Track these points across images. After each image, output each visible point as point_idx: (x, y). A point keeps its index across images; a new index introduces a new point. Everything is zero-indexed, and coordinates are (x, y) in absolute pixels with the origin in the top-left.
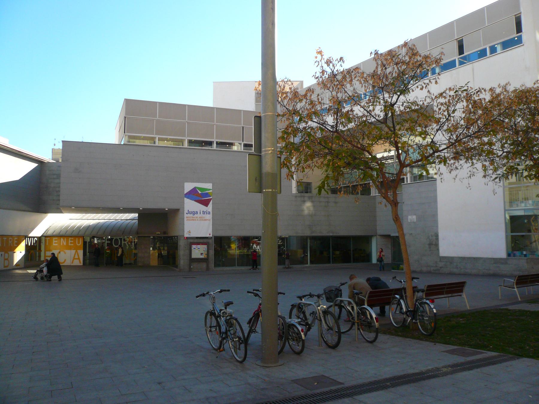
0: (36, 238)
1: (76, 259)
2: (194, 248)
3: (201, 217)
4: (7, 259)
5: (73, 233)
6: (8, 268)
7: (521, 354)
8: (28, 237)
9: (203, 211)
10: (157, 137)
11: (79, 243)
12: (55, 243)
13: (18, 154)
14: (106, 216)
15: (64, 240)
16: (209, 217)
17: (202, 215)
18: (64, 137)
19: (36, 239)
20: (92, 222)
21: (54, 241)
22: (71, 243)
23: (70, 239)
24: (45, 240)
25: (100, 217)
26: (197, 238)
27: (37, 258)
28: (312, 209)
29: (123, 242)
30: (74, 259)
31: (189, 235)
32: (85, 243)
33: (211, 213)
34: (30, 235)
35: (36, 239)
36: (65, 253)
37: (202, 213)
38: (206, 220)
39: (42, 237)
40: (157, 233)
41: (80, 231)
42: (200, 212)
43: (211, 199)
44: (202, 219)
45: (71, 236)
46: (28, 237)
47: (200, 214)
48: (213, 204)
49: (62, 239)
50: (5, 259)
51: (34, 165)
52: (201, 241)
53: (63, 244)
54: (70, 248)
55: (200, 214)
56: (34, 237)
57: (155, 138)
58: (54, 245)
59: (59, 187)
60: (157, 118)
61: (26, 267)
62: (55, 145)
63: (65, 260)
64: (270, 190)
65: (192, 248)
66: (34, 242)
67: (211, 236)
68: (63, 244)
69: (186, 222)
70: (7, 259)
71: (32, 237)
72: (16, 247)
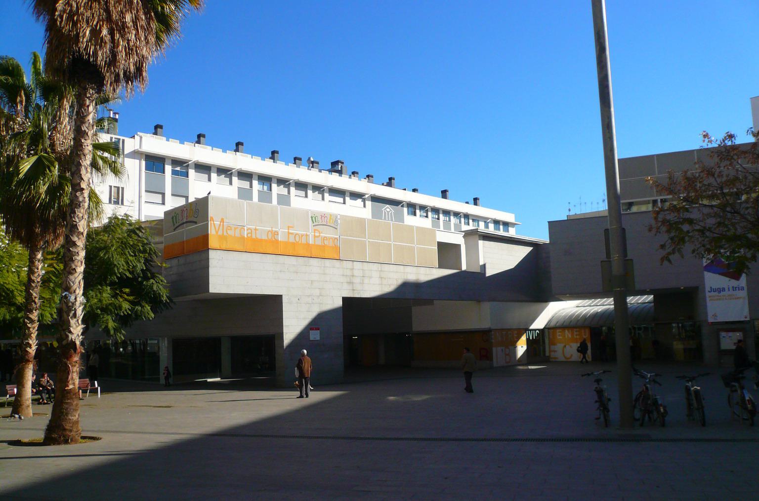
0: (537, 331)
2: (724, 337)
4: (508, 355)
6: (510, 364)
8: (529, 330)
9: (733, 287)
11: (585, 335)
14: (598, 302)
16: (743, 294)
17: (731, 292)
20: (599, 309)
21: (558, 334)
23: (575, 329)
25: (585, 303)
26: (727, 323)
33: (746, 288)
34: (532, 327)
37: (731, 289)
38: (738, 298)
40: (680, 319)
41: (578, 321)
42: (729, 288)
46: (529, 330)
50: (506, 355)
51: (529, 249)
56: (535, 330)
62: (569, 210)
63: (572, 355)
65: (721, 337)
67: (748, 319)
70: (508, 355)
71: (533, 330)
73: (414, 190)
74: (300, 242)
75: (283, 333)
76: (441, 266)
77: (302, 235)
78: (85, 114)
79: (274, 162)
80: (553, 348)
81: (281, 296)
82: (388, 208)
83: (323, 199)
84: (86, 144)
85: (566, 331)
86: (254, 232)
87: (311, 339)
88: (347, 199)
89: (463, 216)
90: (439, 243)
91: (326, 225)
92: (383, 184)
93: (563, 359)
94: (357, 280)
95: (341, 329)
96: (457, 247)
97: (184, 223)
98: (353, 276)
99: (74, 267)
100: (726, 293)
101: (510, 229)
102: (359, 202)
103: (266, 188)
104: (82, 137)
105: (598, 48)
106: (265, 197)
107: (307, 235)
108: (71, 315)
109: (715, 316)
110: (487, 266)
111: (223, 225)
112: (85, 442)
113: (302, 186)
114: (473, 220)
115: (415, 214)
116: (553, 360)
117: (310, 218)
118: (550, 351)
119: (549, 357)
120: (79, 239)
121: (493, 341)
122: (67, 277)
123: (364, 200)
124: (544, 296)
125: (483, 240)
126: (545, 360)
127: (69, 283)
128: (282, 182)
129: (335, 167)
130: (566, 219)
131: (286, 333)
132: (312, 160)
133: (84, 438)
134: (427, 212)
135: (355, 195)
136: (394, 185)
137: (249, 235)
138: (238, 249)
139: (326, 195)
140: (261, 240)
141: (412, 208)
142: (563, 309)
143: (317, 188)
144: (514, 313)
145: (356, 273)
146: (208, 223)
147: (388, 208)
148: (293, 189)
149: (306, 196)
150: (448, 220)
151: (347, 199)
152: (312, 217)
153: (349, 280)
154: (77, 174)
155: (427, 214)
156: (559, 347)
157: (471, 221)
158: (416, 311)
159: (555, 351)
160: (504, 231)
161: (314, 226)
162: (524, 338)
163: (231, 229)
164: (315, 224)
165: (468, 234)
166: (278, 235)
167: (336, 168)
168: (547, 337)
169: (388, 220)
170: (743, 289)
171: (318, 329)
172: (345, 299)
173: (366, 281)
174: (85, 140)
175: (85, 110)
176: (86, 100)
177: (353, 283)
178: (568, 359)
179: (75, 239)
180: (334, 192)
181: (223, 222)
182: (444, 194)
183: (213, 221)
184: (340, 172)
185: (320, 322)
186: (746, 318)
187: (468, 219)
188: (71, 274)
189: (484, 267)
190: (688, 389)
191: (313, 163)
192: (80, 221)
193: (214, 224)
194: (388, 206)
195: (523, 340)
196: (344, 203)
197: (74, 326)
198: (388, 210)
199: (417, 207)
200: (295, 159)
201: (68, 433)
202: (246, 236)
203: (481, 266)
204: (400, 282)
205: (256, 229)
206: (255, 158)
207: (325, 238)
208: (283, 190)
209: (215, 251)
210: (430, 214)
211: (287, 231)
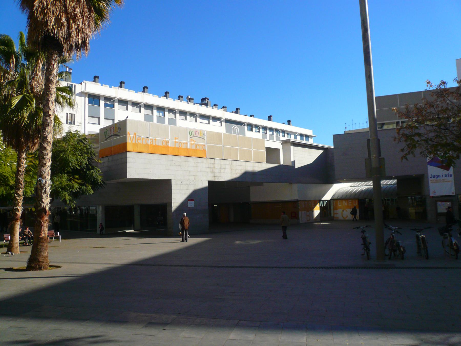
0: (326, 201)
3: (443, 180)
5: (343, 197)
7: (368, 240)
11: (355, 204)
12: (340, 204)
13: (310, 146)
15: (345, 202)
16: (452, 179)
17: (444, 178)
18: (352, 121)
19: (326, 202)
20: (364, 188)
21: (339, 203)
22: (350, 204)
24: (333, 202)
29: (387, 202)
31: (434, 194)
34: (323, 199)
35: (326, 202)
37: (444, 176)
38: (449, 181)
39: (331, 200)
47: (443, 177)
49: (344, 201)
50: (307, 216)
51: (321, 152)
53: (345, 205)
55: (443, 177)
56: (325, 201)
58: (339, 205)
60: (398, 106)
62: (346, 128)
64: (376, 176)
66: (326, 204)
67: (454, 194)
68: (345, 205)
69: (431, 184)
71: (324, 201)
72: (314, 207)
73: (252, 116)
74: (182, 147)
77: (184, 143)
78: (52, 69)
79: (166, 99)
81: (171, 180)
82: (235, 126)
83: (196, 121)
84: (52, 88)
86: (154, 141)
88: (211, 121)
90: (266, 147)
91: (198, 137)
92: (232, 112)
94: (216, 171)
96: (277, 150)
97: (111, 136)
99: (45, 162)
101: (310, 139)
103: (161, 114)
104: (50, 83)
107: (186, 143)
108: (43, 191)
109: (434, 192)
110: (296, 162)
111: (135, 137)
113: (183, 113)
114: (287, 134)
115: (252, 131)
116: (336, 219)
117: (188, 133)
118: (334, 214)
119: (333, 217)
120: (48, 145)
121: (299, 207)
122: (41, 169)
123: (221, 122)
125: (293, 146)
127: (42, 172)
128: (171, 111)
129: (204, 102)
132: (189, 97)
134: (259, 129)
135: (216, 119)
136: (239, 112)
137: (151, 143)
139: (198, 119)
141: (250, 126)
142: (342, 188)
143: (193, 115)
146: (126, 136)
147: (235, 127)
148: (178, 115)
149: (186, 120)
150: (272, 134)
151: (211, 121)
152: (189, 132)
153: (212, 171)
156: (340, 211)
157: (286, 135)
158: (252, 189)
159: (337, 214)
162: (318, 206)
167: (204, 102)
171: (193, 200)
173: (222, 171)
174: (52, 85)
175: (52, 67)
177: (214, 172)
180: (203, 117)
181: (136, 135)
182: (270, 118)
183: (129, 135)
184: (206, 105)
186: (453, 193)
187: (284, 133)
188: (43, 166)
190: (418, 237)
191: (190, 99)
193: (130, 136)
194: (235, 125)
197: (45, 198)
198: (236, 128)
199: (253, 126)
200: (179, 97)
202: (149, 144)
203: (292, 162)
204: (243, 171)
205: (155, 140)
206: (104, 86)
207: (197, 145)
208: (172, 116)
209: (130, 153)
210: (261, 130)
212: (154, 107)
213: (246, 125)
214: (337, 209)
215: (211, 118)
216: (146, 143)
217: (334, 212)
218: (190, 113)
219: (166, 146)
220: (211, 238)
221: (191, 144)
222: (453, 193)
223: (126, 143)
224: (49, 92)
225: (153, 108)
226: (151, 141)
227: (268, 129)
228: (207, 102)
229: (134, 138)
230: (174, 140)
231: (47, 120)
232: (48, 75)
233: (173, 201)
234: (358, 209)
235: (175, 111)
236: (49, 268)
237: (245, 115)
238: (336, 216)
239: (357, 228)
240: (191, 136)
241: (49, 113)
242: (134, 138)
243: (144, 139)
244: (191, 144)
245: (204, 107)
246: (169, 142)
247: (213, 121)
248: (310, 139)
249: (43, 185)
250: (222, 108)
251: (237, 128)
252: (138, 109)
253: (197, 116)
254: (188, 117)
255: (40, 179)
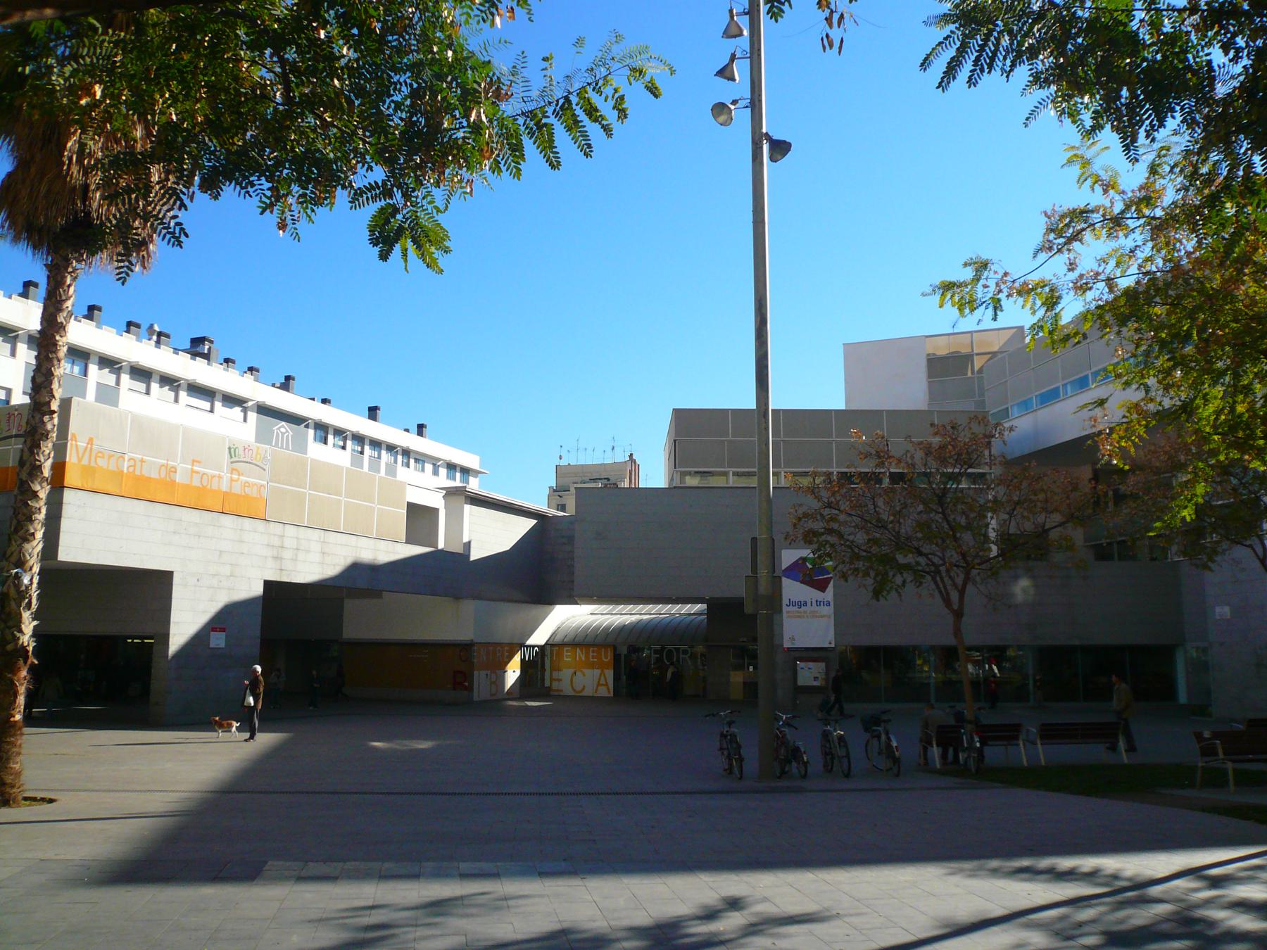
1: (602, 685)
3: (814, 612)
6: (495, 698)
10: (731, 470)
11: (606, 658)
12: (567, 657)
15: (582, 651)
17: (815, 608)
20: (629, 619)
21: (565, 653)
22: (593, 657)
23: (591, 649)
24: (552, 652)
26: (807, 649)
27: (539, 682)
28: (1032, 591)
29: (681, 656)
30: (599, 685)
31: (793, 644)
32: (617, 658)
33: (832, 603)
34: (529, 642)
36: (584, 675)
38: (822, 617)
40: (741, 640)
43: (831, 578)
44: (814, 615)
45: (593, 645)
48: (834, 586)
51: (531, 523)
52: (815, 655)
54: (592, 666)
56: (534, 647)
57: (728, 472)
59: (573, 559)
61: (524, 697)
67: (833, 646)
71: (530, 646)
73: (324, 401)
74: (209, 487)
75: (169, 634)
76: (409, 540)
77: (213, 477)
78: (64, 298)
79: (208, 364)
80: (555, 675)
81: (172, 572)
82: (283, 426)
83: (176, 400)
84: (60, 343)
85: (578, 649)
86: (138, 464)
87: (211, 646)
88: (218, 405)
89: (400, 452)
90: (409, 504)
91: (250, 463)
92: (273, 385)
93: (573, 694)
94: (287, 555)
95: (258, 633)
96: (435, 511)
97: (11, 437)
98: (282, 547)
99: (32, 531)
100: (808, 609)
101: (471, 479)
102: (237, 410)
103: (77, 369)
104: (58, 332)
105: (759, 319)
106: (375, 461)
107: (220, 477)
108: (23, 604)
109: (793, 639)
110: (472, 543)
111: (91, 449)
112: (29, 806)
113: (142, 374)
114: (416, 460)
115: (325, 442)
116: (556, 693)
117: (227, 450)
118: (552, 680)
119: (549, 688)
120: (42, 488)
121: (475, 661)
122: (20, 547)
123: (245, 410)
124: (547, 596)
125: (471, 504)
126: (545, 694)
127: (24, 555)
128: (108, 362)
129: (198, 348)
130: (197, 358)
131: (175, 635)
132: (157, 328)
133: (26, 799)
134: (345, 439)
135: (232, 400)
136: (293, 388)
137: (131, 469)
138: (110, 489)
139: (183, 394)
140: (149, 479)
141: (323, 430)
142: (573, 617)
143: (168, 381)
144: (507, 618)
145: (288, 543)
146: (66, 444)
147: (283, 427)
148: (125, 378)
149: (148, 393)
150: (376, 456)
151: (218, 405)
152: (230, 448)
153: (275, 554)
154: (45, 388)
155: (363, 449)
156: (565, 674)
157: (412, 461)
158: (350, 605)
159: (559, 680)
160: (461, 481)
161: (232, 463)
162: (517, 659)
163: (103, 457)
164: (234, 459)
165: (450, 493)
166: (176, 472)
167: (199, 349)
168: (549, 656)
169: (282, 448)
170: (829, 604)
171: (223, 630)
172: (268, 585)
173: (301, 556)
174: (61, 336)
175: (64, 291)
176: (66, 277)
177: (281, 559)
178: (577, 692)
179: (36, 487)
180: (197, 390)
181: (92, 444)
182: (373, 413)
183: (76, 441)
184: (207, 357)
185: (226, 618)
186: (830, 643)
187: (409, 458)
188: (28, 541)
189: (468, 545)
190: (826, 735)
191: (160, 334)
192: (46, 460)
193: (77, 445)
194: (283, 423)
195: (517, 659)
196: (212, 411)
197: (27, 623)
198: (283, 430)
199: (331, 431)
200: (129, 324)
201: (8, 790)
202: (125, 471)
203: (465, 544)
204: (349, 561)
205: (142, 461)
206: (106, 330)
207: (246, 484)
208: (108, 377)
209: (73, 492)
210: (349, 443)
211: (190, 467)
212: (92, 357)
213: (312, 425)
214: (559, 670)
215: (219, 396)
216: (118, 468)
217: (551, 675)
218: (223, 395)
219: (168, 479)
220: (285, 734)
221: (232, 480)
222: (830, 643)
223: (64, 463)
224: (54, 352)
225: (215, 396)
226: (132, 463)
227: (367, 442)
228: (209, 349)
229: (88, 449)
230: (190, 467)
231: (43, 423)
232: (52, 309)
233: (173, 630)
234: (612, 672)
235: (16, 333)
236: (23, 802)
237: (311, 399)
238: (555, 685)
239: (713, 715)
240: (232, 460)
241: (50, 407)
242: (88, 449)
243: (113, 456)
244: (232, 480)
245: (201, 362)
246: (176, 469)
247: (131, 378)
248: (471, 479)
249: (23, 588)
250: (222, 362)
251: (287, 431)
252: (9, 346)
253: (179, 385)
254: (155, 386)
255: (17, 573)
